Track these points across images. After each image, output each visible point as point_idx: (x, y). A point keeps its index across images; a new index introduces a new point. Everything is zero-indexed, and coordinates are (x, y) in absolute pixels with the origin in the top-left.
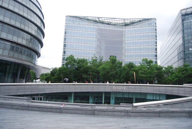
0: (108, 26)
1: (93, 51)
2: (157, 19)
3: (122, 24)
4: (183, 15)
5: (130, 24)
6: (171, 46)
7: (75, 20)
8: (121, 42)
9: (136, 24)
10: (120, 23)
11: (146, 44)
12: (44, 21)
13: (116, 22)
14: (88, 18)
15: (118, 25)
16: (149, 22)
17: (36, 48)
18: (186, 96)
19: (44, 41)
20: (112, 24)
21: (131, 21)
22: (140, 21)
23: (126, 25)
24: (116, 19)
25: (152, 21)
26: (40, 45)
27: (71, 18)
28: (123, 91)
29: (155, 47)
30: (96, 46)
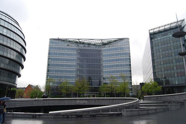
4: (151, 34)
8: (99, 60)
10: (99, 43)
14: (70, 40)
16: (123, 41)
19: (26, 56)
21: (108, 41)
22: (116, 41)
23: (104, 44)
24: (93, 39)
26: (23, 58)
28: (85, 104)
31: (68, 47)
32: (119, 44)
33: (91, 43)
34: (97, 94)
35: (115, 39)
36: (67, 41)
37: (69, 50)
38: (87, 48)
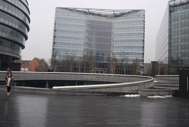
0: (98, 17)
2: (145, 11)
4: (170, 7)
7: (65, 11)
8: (110, 34)
9: (126, 15)
11: (134, 35)
13: (106, 13)
14: (78, 9)
15: (109, 16)
16: (138, 13)
17: (19, 41)
19: (29, 34)
21: (120, 12)
22: (129, 13)
23: (116, 16)
25: (141, 12)
27: (61, 10)
28: (93, 80)
30: (85, 37)
35: (130, 10)
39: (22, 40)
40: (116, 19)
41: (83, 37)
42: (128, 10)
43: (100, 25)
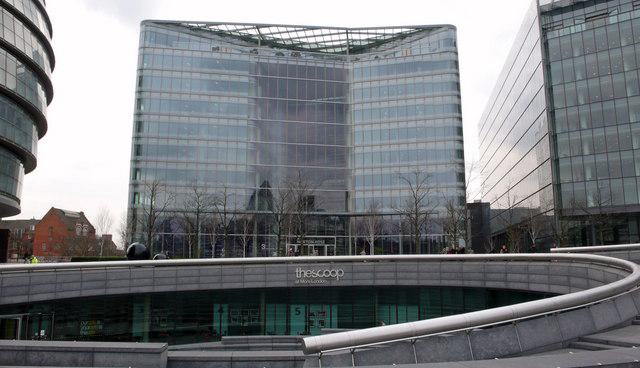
1: (240, 145)
3: (341, 46)
4: (543, 13)
5: (370, 46)
6: (501, 119)
7: (176, 34)
12: (53, 43)
16: (434, 37)
17: (16, 139)
18: (555, 292)
19: (50, 113)
20: (307, 47)
21: (370, 36)
22: (402, 36)
23: (356, 50)
28: (334, 284)
29: (456, 123)
31: (216, 55)
32: (421, 48)
33: (304, 43)
34: (327, 241)
35: (401, 27)
36: (211, 31)
37: (219, 67)
38: (318, 65)
39: (27, 136)
40: (357, 59)
41: (244, 123)
42: (397, 28)
43: (300, 82)
